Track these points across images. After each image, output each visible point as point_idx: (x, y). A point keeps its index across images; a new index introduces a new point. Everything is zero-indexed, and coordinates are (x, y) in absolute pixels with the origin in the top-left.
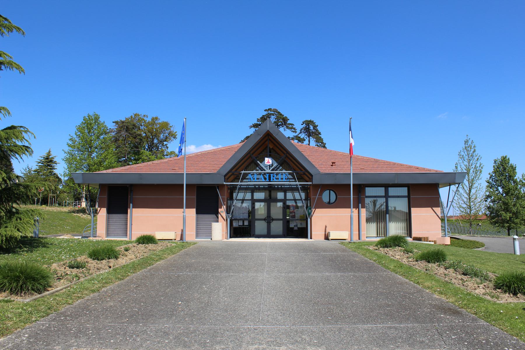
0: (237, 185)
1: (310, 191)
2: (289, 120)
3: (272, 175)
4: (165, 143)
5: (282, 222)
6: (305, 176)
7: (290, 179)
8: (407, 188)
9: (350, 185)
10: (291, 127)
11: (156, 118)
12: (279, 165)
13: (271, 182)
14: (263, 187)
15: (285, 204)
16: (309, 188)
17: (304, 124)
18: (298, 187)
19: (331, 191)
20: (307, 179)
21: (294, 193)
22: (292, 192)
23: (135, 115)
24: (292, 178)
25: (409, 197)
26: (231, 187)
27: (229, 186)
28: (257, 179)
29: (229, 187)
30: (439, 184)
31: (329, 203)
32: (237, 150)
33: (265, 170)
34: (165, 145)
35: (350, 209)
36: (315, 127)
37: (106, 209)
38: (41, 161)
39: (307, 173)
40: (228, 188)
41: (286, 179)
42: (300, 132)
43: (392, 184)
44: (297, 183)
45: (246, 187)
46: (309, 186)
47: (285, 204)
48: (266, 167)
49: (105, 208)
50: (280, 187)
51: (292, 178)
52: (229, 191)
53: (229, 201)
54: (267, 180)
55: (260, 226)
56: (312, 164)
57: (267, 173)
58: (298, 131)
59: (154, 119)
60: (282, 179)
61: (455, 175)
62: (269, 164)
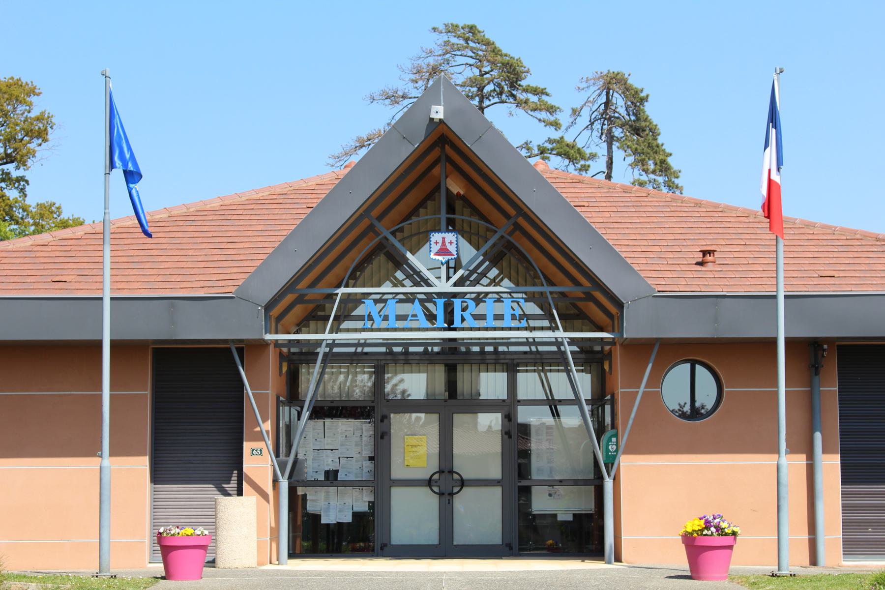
0: (318, 343)
3: (457, 303)
5: (497, 491)
7: (525, 316)
9: (98, 344)
13: (455, 329)
15: (510, 420)
16: (609, 355)
18: (564, 353)
22: (539, 372)
26: (293, 350)
27: (283, 345)
28: (400, 318)
29: (285, 350)
36: (637, 100)
39: (598, 295)
40: (282, 357)
44: (561, 334)
46: (607, 348)
47: (510, 420)
52: (285, 369)
53: (287, 408)
54: (441, 322)
57: (440, 295)
60: (499, 317)
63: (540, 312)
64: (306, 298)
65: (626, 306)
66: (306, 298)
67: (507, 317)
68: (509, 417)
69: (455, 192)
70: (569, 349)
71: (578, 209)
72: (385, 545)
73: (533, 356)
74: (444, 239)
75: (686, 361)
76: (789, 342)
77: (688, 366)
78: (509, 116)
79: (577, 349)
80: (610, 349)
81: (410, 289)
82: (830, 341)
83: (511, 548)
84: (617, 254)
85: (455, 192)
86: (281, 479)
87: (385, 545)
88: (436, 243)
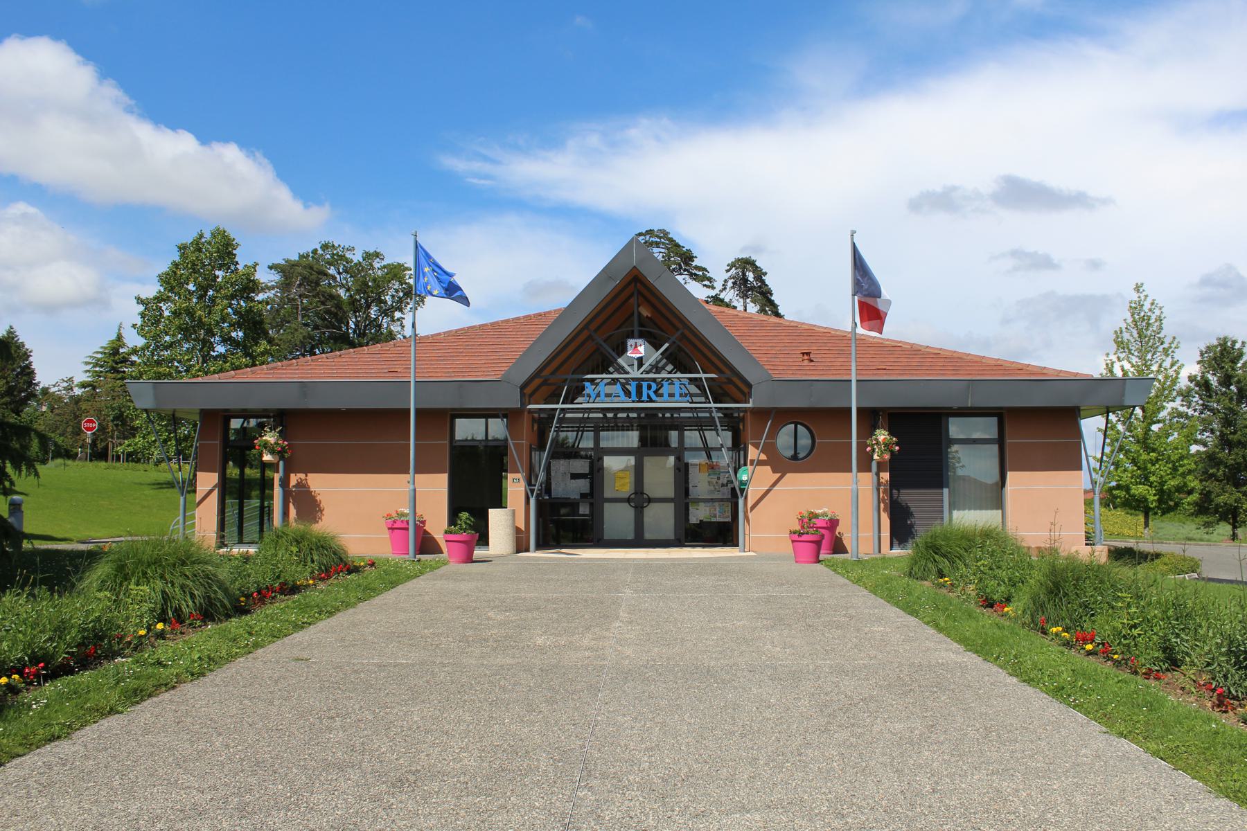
1: (744, 427)
2: (696, 257)
3: (645, 385)
4: (397, 315)
5: (671, 506)
6: (731, 386)
7: (691, 395)
8: (996, 419)
9: (850, 410)
10: (702, 276)
11: (377, 255)
12: (665, 361)
13: (643, 402)
14: (600, 415)
15: (680, 461)
16: (743, 420)
17: (731, 269)
18: (714, 418)
19: (799, 426)
20: (738, 395)
21: (705, 432)
22: (699, 430)
23: (325, 247)
24: (780, 474)
25: (1001, 441)
26: (542, 416)
27: (535, 412)
28: (607, 395)
29: (536, 415)
30: (1081, 408)
31: (795, 457)
32: (552, 320)
33: (628, 373)
34: (398, 320)
35: (1000, 511)
36: (760, 275)
37: (217, 474)
38: (98, 360)
39: (735, 379)
40: (534, 420)
41: (681, 395)
42: (721, 287)
43: (960, 408)
44: (712, 405)
45: (581, 415)
46: (741, 414)
47: (680, 461)
48: (631, 365)
49: (214, 471)
50: (668, 415)
51: (780, 474)
52: (536, 427)
53: (537, 453)
55: (617, 518)
56: (752, 356)
57: (633, 379)
58: (718, 285)
59: (370, 256)
60: (672, 395)
61: (1124, 384)
62: (638, 355)
63: (699, 392)
64: (549, 382)
65: (753, 387)
66: (549, 382)
67: (677, 395)
68: (679, 459)
69: (645, 315)
70: (717, 415)
71: (727, 328)
72: (600, 539)
73: (695, 420)
74: (636, 343)
75: (791, 423)
76: (859, 410)
77: (793, 425)
78: (800, 513)
79: (722, 416)
80: (744, 416)
81: (616, 376)
82: (883, 410)
83: (680, 542)
84: (750, 356)
85: (645, 315)
86: (530, 496)
87: (600, 539)
88: (631, 346)
